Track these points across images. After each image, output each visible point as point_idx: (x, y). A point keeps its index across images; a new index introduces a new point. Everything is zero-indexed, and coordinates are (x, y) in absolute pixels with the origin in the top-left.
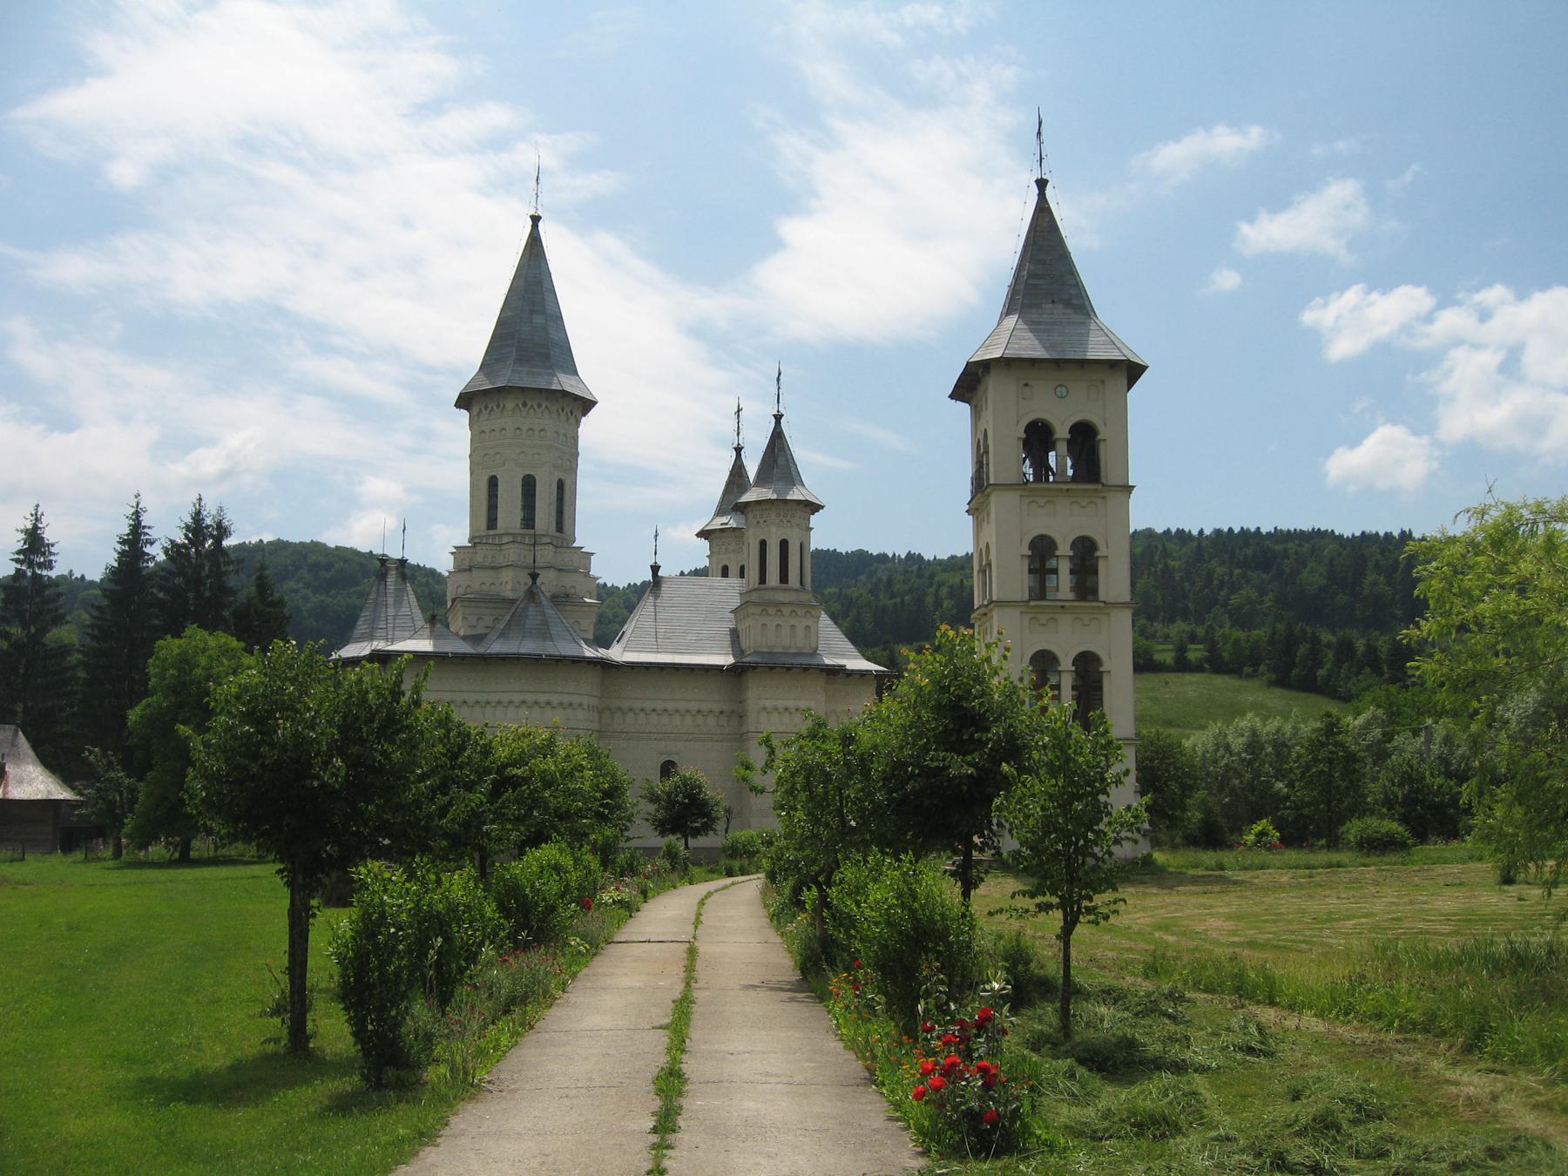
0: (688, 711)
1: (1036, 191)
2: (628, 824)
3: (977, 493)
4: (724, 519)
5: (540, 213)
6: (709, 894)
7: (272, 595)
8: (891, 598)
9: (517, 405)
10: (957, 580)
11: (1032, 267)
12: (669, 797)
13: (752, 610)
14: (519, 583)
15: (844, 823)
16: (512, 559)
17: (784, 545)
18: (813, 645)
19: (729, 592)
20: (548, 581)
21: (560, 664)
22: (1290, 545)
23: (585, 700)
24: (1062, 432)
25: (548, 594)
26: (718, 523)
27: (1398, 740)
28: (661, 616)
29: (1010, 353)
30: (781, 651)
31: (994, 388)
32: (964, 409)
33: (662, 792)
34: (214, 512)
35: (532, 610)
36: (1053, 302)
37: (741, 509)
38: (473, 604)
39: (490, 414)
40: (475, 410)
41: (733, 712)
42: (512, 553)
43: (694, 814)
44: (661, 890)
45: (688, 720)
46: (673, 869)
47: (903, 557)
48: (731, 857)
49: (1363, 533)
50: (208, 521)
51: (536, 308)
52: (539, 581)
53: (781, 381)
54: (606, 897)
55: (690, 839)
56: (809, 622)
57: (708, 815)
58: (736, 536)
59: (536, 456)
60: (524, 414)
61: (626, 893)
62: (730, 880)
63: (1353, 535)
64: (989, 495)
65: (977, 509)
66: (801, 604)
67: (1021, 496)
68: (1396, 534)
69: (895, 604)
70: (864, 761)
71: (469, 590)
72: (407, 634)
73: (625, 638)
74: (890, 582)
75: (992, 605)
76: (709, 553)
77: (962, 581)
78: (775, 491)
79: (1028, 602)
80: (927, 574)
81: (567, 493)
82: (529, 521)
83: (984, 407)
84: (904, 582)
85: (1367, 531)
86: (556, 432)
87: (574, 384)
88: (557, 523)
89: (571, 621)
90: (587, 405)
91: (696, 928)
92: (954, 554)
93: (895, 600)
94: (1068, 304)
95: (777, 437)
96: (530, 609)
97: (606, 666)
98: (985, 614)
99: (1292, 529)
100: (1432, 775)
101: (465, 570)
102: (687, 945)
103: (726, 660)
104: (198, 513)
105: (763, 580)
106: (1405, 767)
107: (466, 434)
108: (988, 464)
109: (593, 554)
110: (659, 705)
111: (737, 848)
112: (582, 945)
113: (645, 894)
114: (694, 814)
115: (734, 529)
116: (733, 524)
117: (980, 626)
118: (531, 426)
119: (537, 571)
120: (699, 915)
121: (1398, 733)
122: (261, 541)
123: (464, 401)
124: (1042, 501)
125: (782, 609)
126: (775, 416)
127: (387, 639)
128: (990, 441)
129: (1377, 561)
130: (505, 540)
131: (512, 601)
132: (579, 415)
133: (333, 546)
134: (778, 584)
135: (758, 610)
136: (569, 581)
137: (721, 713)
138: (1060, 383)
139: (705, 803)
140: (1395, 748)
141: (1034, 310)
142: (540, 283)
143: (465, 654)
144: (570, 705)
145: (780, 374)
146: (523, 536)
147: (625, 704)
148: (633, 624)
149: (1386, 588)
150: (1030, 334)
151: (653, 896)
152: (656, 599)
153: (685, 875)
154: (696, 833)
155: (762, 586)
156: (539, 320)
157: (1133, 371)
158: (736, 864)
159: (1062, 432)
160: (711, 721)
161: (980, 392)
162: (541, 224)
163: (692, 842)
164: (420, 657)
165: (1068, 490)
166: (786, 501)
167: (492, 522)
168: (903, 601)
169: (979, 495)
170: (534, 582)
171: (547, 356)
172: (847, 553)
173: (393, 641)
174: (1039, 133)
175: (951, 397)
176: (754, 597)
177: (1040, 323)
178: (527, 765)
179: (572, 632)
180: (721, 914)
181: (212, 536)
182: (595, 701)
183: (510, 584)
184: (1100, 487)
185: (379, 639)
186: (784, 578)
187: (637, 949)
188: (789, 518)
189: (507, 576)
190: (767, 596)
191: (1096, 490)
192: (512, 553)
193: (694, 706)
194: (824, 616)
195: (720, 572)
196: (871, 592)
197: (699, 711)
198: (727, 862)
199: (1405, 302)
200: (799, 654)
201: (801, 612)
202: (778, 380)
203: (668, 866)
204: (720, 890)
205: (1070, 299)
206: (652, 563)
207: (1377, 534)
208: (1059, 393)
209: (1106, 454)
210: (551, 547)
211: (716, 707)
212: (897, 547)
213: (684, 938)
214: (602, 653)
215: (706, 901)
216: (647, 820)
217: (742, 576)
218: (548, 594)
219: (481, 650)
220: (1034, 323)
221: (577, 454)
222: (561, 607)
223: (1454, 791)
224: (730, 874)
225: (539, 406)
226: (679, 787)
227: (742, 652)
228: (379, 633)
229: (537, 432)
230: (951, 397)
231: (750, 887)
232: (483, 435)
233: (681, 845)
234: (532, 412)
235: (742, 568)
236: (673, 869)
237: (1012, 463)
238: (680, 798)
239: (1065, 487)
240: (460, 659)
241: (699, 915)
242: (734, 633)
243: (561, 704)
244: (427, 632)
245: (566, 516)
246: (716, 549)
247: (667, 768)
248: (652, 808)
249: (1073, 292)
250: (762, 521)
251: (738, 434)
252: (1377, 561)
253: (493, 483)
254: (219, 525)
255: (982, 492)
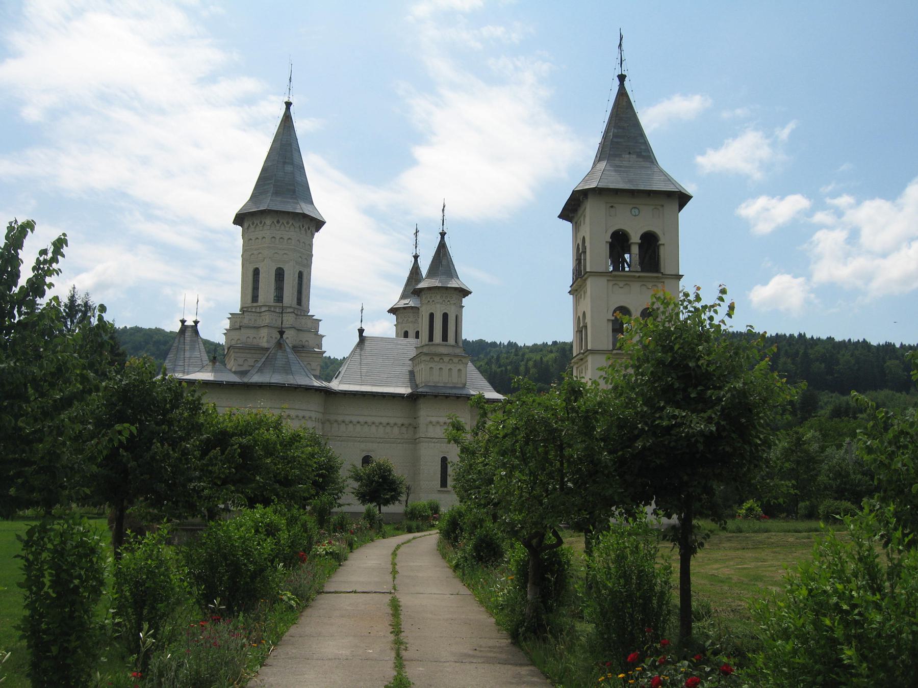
0: (381, 423)
1: (618, 83)
2: (340, 494)
3: (577, 279)
4: (406, 301)
5: (291, 101)
6: (398, 547)
7: (118, 349)
8: (499, 367)
9: (273, 222)
10: (538, 358)
11: (616, 131)
12: (369, 477)
13: (423, 358)
14: (271, 337)
15: (563, 484)
16: (267, 321)
17: (445, 316)
18: (463, 381)
19: (410, 347)
20: (290, 337)
21: (298, 390)
22: (735, 340)
23: (313, 415)
24: (635, 238)
25: (290, 345)
26: (402, 304)
27: (829, 451)
28: (364, 362)
29: (601, 185)
30: (442, 385)
31: (590, 208)
32: (568, 226)
33: (364, 474)
34: (83, 296)
35: (280, 354)
36: (630, 153)
37: (418, 293)
38: (241, 351)
39: (255, 227)
40: (246, 225)
41: (410, 425)
42: (267, 319)
43: (385, 490)
44: (363, 543)
45: (381, 429)
46: (371, 527)
47: (506, 344)
48: (410, 519)
49: (777, 334)
50: (79, 302)
51: (287, 161)
52: (285, 336)
53: (445, 211)
54: (321, 550)
55: (382, 507)
56: (460, 367)
57: (395, 490)
58: (413, 313)
59: (285, 256)
60: (278, 228)
61: (337, 546)
62: (411, 536)
63: (771, 335)
64: (585, 280)
65: (577, 290)
66: (456, 356)
67: (608, 280)
68: (796, 335)
69: (502, 371)
70: (588, 419)
71: (239, 342)
72: (197, 369)
73: (341, 375)
74: (498, 359)
75: (587, 353)
76: (396, 323)
77: (541, 358)
78: (440, 281)
79: (612, 351)
80: (520, 353)
81: (305, 281)
82: (279, 298)
83: (582, 224)
84: (507, 358)
85: (780, 333)
86: (298, 240)
87: (311, 210)
88: (298, 299)
89: (305, 363)
90: (318, 224)
91: (394, 578)
92: (536, 343)
93: (501, 369)
94: (639, 155)
95: (442, 247)
96: (279, 354)
97: (329, 393)
98: (582, 359)
99: (735, 332)
100: (854, 473)
101: (237, 329)
102: (389, 597)
103: (405, 390)
104: (73, 296)
105: (431, 338)
106: (837, 468)
107: (240, 242)
108: (585, 260)
109: (321, 320)
110: (362, 419)
111: (415, 513)
112: (293, 599)
113: (351, 546)
114: (385, 490)
115: (412, 308)
116: (412, 304)
117: (577, 368)
118: (282, 236)
119: (284, 330)
120: (394, 564)
121: (828, 447)
122: (126, 327)
123: (239, 219)
124: (621, 284)
125: (443, 358)
126: (440, 233)
127: (184, 372)
128: (587, 244)
129: (786, 351)
130: (263, 309)
131: (267, 349)
132: (314, 230)
133: (168, 331)
134: (441, 342)
135: (428, 358)
136: (306, 338)
137: (402, 425)
138: (634, 206)
139: (393, 482)
140: (826, 457)
141: (617, 159)
142: (290, 145)
143: (235, 382)
144: (303, 417)
145: (444, 207)
146: (275, 307)
147: (340, 418)
148: (346, 367)
149: (792, 366)
150: (613, 173)
151: (357, 548)
152: (361, 351)
153: (380, 531)
154: (387, 502)
155: (431, 343)
156: (289, 168)
157: (683, 199)
158: (414, 524)
159: (635, 238)
160: (396, 430)
161: (580, 212)
162: (292, 107)
163: (384, 509)
164: (206, 384)
165: (639, 277)
166: (447, 288)
167: (255, 298)
168: (506, 369)
169: (579, 280)
170: (282, 337)
171: (294, 191)
172: (473, 341)
173: (188, 374)
174: (620, 45)
175: (560, 217)
176: (425, 350)
177: (620, 167)
178: (251, 435)
179: (306, 371)
180: (412, 564)
181: (81, 311)
182: (320, 416)
183: (265, 338)
184: (660, 275)
185: (179, 372)
186: (445, 337)
187: (345, 602)
188: (449, 299)
189: (264, 332)
190: (434, 350)
191: (657, 277)
192: (267, 319)
193: (384, 420)
194: (470, 364)
195: (403, 335)
196: (487, 363)
197: (388, 424)
198: (408, 522)
199: (795, 203)
200: (455, 388)
201: (456, 360)
202: (443, 210)
203: (369, 526)
204: (405, 543)
205: (641, 152)
206: (359, 327)
207: (785, 335)
208: (633, 213)
209: (664, 253)
210: (294, 315)
211: (399, 421)
212: (502, 338)
213: (385, 588)
214: (325, 384)
215: (397, 552)
216: (353, 493)
217: (417, 336)
218: (290, 345)
219: (246, 380)
220: (617, 166)
221: (312, 256)
222: (298, 354)
223: (868, 483)
224: (410, 531)
225: (288, 223)
226: (376, 471)
227: (417, 386)
228: (179, 368)
229: (285, 241)
230: (560, 217)
231: (430, 538)
232: (250, 241)
233: (376, 510)
234: (283, 227)
235: (417, 333)
236: (371, 527)
237: (598, 258)
238: (376, 478)
239: (638, 274)
240: (231, 386)
241: (394, 564)
242: (412, 373)
243: (297, 416)
244: (210, 368)
245: (303, 296)
246: (400, 321)
247: (366, 460)
248: (356, 485)
249: (643, 147)
250: (431, 301)
251: (416, 247)
252: (786, 351)
253: (256, 272)
254: (86, 304)
255: (581, 278)
